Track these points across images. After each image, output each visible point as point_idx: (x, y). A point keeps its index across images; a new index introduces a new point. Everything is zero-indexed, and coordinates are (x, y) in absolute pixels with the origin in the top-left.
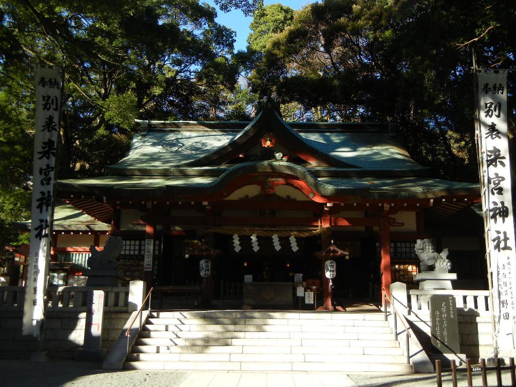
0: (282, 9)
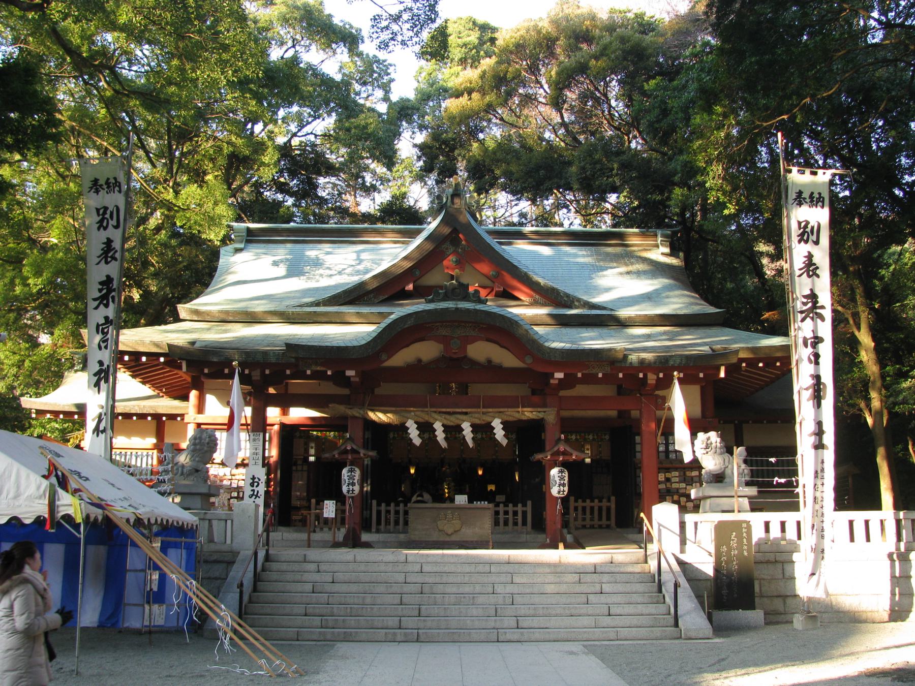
0: (474, 23)
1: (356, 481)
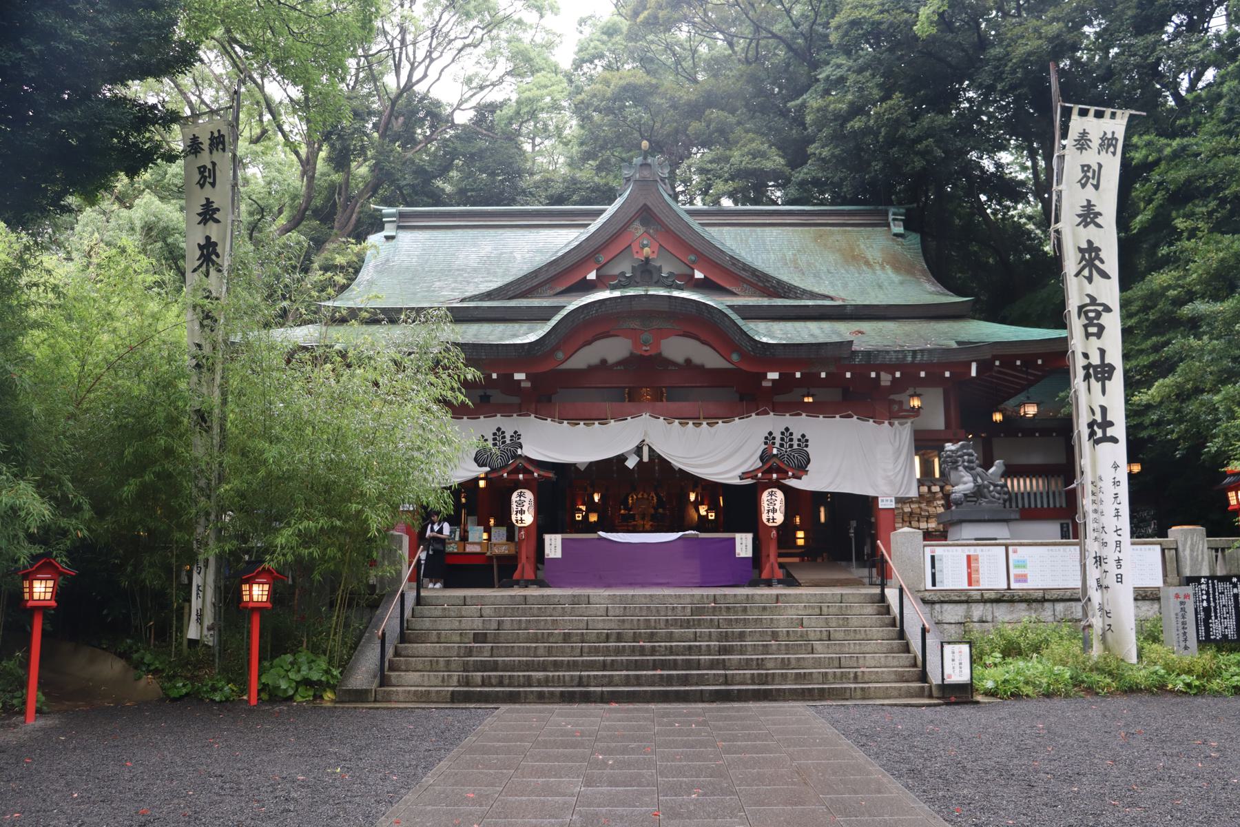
1: (525, 508)
